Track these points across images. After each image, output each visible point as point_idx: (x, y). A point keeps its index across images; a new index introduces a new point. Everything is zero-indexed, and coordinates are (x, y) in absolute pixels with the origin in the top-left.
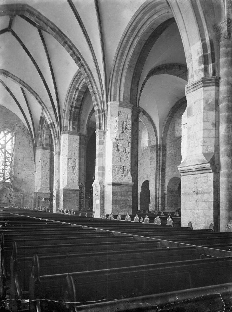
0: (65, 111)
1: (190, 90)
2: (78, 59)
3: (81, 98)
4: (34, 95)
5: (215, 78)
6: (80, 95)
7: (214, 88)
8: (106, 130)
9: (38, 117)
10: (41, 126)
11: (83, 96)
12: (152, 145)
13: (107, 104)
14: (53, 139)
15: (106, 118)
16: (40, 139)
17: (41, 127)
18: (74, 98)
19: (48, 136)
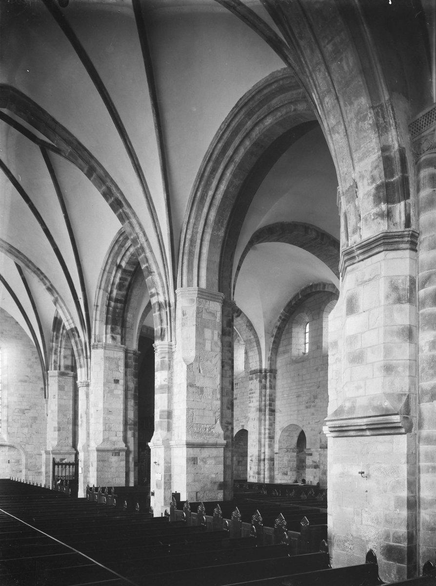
0: (97, 306)
1: (354, 258)
2: (118, 204)
3: (127, 283)
4: (38, 276)
5: (410, 232)
6: (124, 276)
7: (407, 253)
8: (173, 343)
9: (49, 321)
10: (55, 333)
11: (129, 279)
12: (253, 369)
13: (175, 293)
14: (77, 358)
15: (172, 320)
16: (53, 357)
17: (56, 335)
18: (113, 284)
19: (69, 352)
